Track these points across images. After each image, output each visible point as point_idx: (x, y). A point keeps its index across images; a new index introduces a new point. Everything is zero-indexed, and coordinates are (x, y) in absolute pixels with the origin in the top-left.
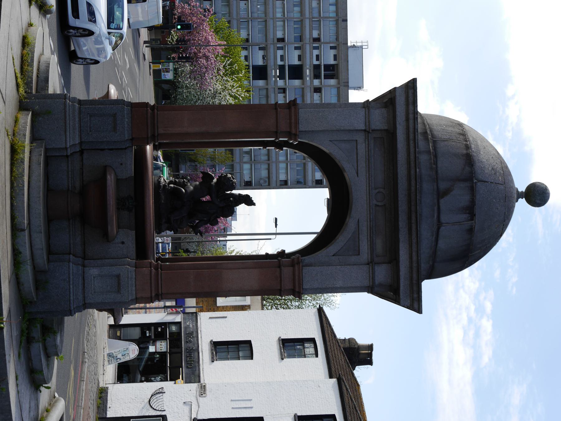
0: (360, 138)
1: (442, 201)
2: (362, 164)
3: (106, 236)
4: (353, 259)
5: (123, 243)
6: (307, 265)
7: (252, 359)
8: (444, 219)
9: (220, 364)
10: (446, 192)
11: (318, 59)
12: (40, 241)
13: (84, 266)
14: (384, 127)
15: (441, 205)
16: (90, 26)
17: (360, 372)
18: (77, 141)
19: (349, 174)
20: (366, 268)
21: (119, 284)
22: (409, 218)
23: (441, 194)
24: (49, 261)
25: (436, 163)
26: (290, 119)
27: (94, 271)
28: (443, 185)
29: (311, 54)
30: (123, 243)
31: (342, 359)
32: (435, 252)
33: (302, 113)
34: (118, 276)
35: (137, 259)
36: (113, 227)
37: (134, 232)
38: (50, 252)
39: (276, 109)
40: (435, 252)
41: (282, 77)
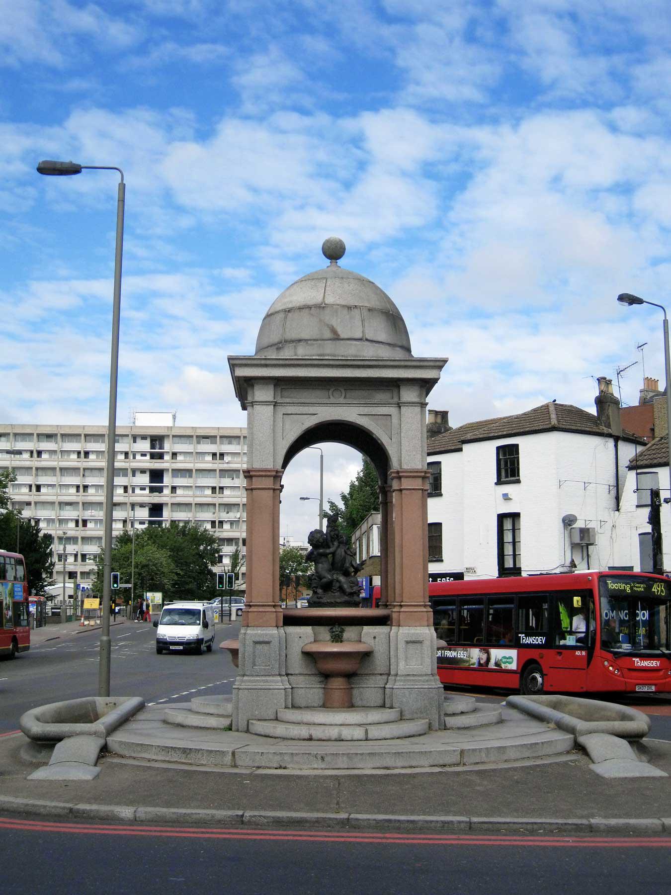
0: (281, 410)
1: (342, 336)
2: (305, 409)
3: (366, 656)
4: (395, 420)
5: (375, 638)
6: (400, 465)
7: (440, 524)
8: (359, 335)
9: (445, 556)
10: (334, 331)
11: (145, 455)
12: (375, 716)
13: (396, 675)
14: (272, 387)
15: (346, 337)
16: (275, 642)
17: (454, 423)
18: (279, 678)
19: (310, 422)
20: (403, 409)
21: (414, 642)
22: (359, 367)
23: (336, 337)
24: (391, 708)
25: (306, 340)
26: (262, 476)
27: (402, 667)
28: (328, 334)
29: (140, 461)
30: (375, 638)
31: (442, 440)
32: (389, 344)
33: (257, 465)
34: (407, 642)
35: (391, 625)
36: (361, 648)
37: (365, 627)
38: (383, 706)
39: (252, 489)
40: (389, 344)
41: (160, 490)
